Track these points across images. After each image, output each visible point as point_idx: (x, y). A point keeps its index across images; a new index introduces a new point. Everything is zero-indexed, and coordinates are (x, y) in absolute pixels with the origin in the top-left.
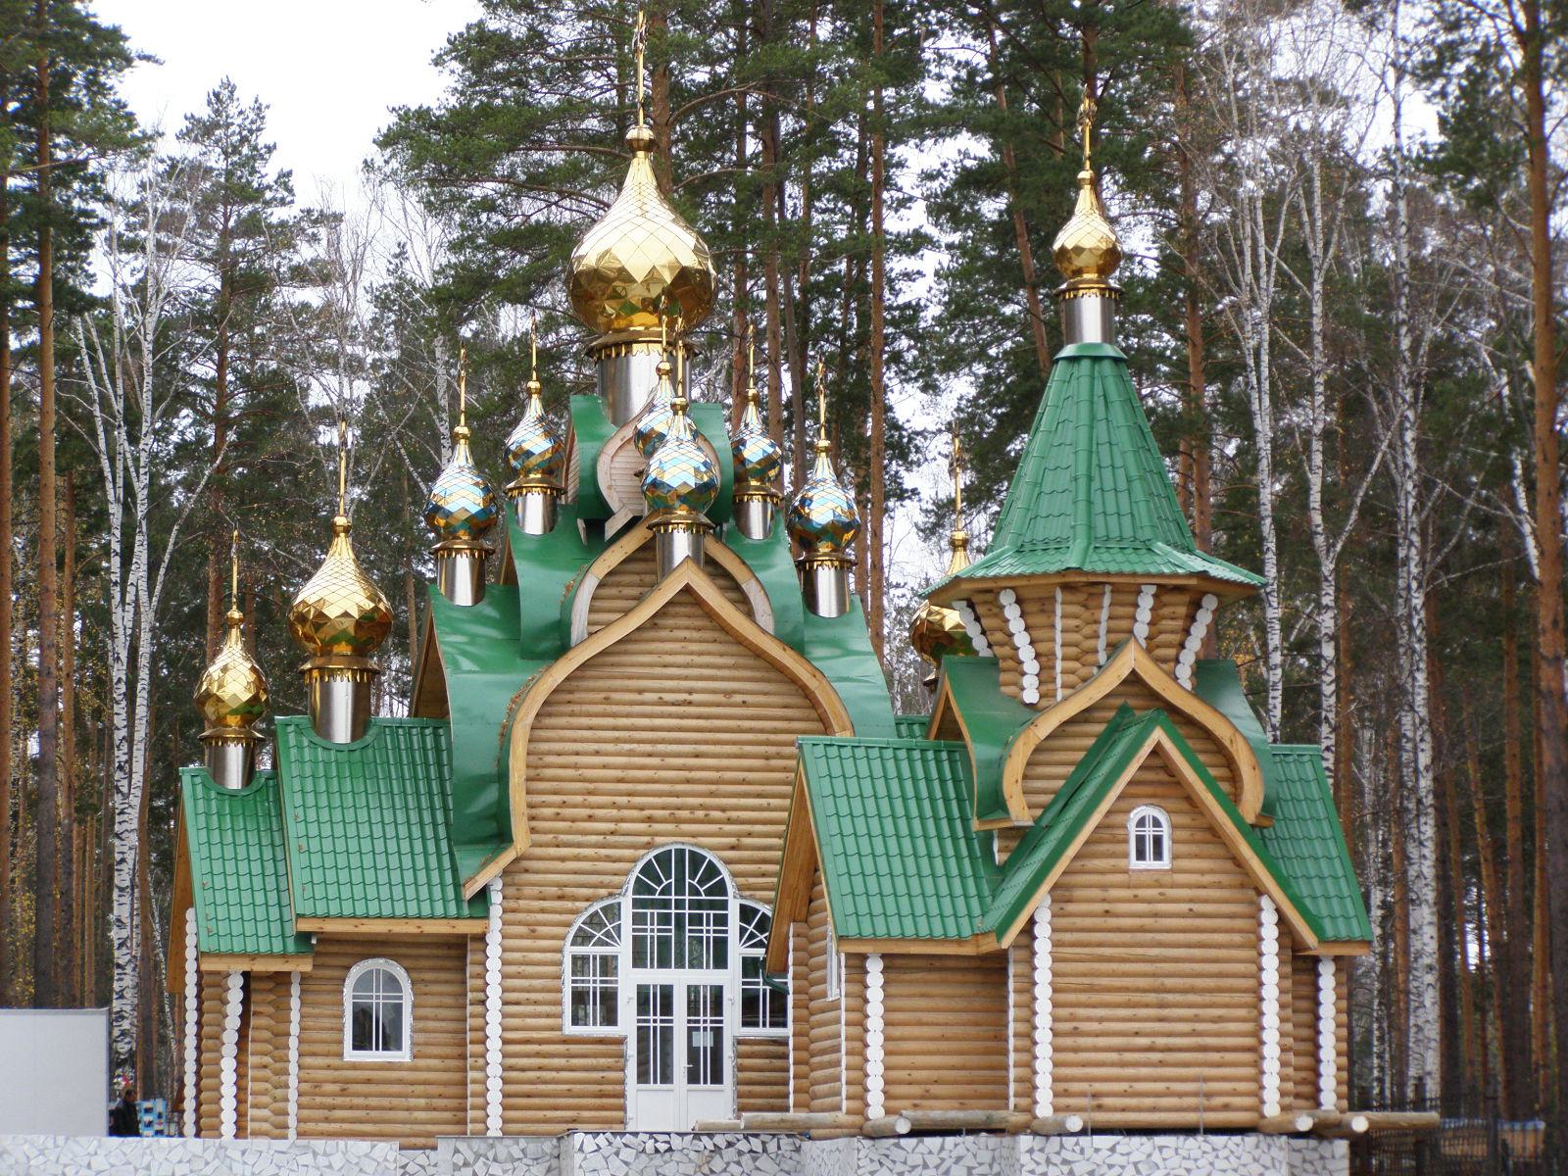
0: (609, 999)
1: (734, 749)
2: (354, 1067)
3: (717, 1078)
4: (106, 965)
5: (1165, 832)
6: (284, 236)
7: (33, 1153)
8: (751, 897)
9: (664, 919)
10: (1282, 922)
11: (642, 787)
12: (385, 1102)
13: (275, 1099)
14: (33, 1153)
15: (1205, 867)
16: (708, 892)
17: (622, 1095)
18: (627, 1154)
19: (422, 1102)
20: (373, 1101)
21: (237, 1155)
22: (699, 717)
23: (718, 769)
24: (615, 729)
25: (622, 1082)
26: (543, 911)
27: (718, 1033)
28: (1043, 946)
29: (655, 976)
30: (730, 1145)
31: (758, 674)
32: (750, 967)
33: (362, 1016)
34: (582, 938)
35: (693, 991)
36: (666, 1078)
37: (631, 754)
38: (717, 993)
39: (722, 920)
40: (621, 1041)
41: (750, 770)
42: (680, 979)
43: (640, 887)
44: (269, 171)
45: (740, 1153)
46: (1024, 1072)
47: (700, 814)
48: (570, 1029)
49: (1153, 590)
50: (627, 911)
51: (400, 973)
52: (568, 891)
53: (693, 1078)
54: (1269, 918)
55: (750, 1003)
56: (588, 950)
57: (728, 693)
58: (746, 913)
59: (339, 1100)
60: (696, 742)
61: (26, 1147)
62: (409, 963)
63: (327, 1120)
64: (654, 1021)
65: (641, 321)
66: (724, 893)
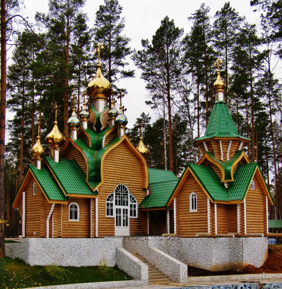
1: (129, 168)
2: (71, 222)
3: (127, 225)
5: (254, 184)
7: (59, 242)
8: (132, 194)
9: (119, 197)
11: (117, 173)
12: (75, 229)
13: (58, 228)
14: (59, 242)
16: (126, 193)
17: (114, 228)
18: (156, 240)
19: (81, 229)
20: (74, 229)
21: (96, 242)
22: (124, 162)
23: (127, 171)
24: (113, 163)
25: (114, 226)
26: (103, 194)
27: (127, 217)
29: (118, 207)
30: (170, 238)
31: (131, 155)
34: (108, 200)
35: (124, 210)
36: (120, 225)
37: (115, 167)
38: (127, 210)
39: (127, 198)
40: (114, 218)
41: (131, 172)
42: (122, 207)
43: (116, 191)
45: (171, 240)
46: (94, 224)
47: (125, 179)
48: (107, 216)
49: (243, 142)
50: (114, 195)
51: (77, 205)
52: (107, 191)
53: (124, 225)
56: (109, 202)
57: (128, 158)
59: (68, 229)
60: (124, 166)
61: (58, 241)
62: (79, 203)
63: (66, 232)
64: (118, 214)
65: (100, 95)
66: (127, 193)
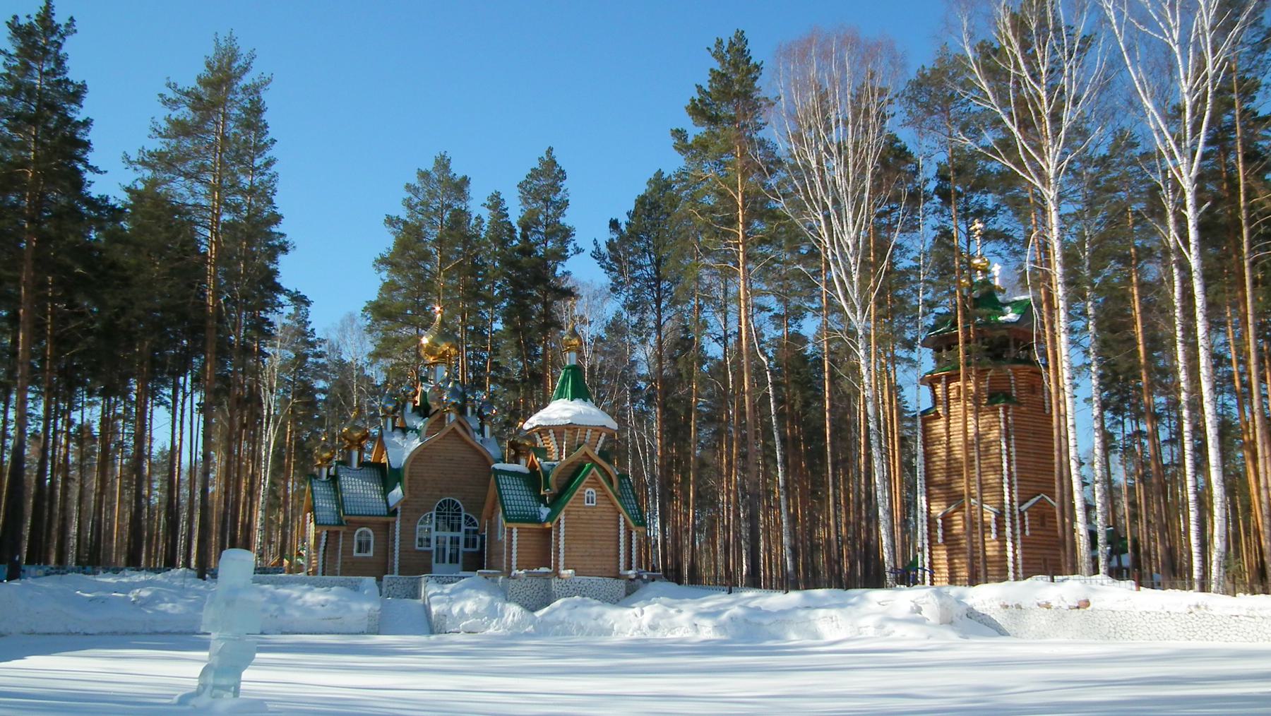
0: (428, 540)
3: (457, 562)
4: (248, 528)
6: (313, 345)
10: (625, 521)
15: (605, 505)
28: (562, 526)
32: (467, 531)
33: (360, 544)
38: (458, 539)
40: (431, 552)
44: (309, 329)
51: (370, 532)
53: (451, 562)
54: (622, 520)
55: (466, 540)
58: (466, 517)
